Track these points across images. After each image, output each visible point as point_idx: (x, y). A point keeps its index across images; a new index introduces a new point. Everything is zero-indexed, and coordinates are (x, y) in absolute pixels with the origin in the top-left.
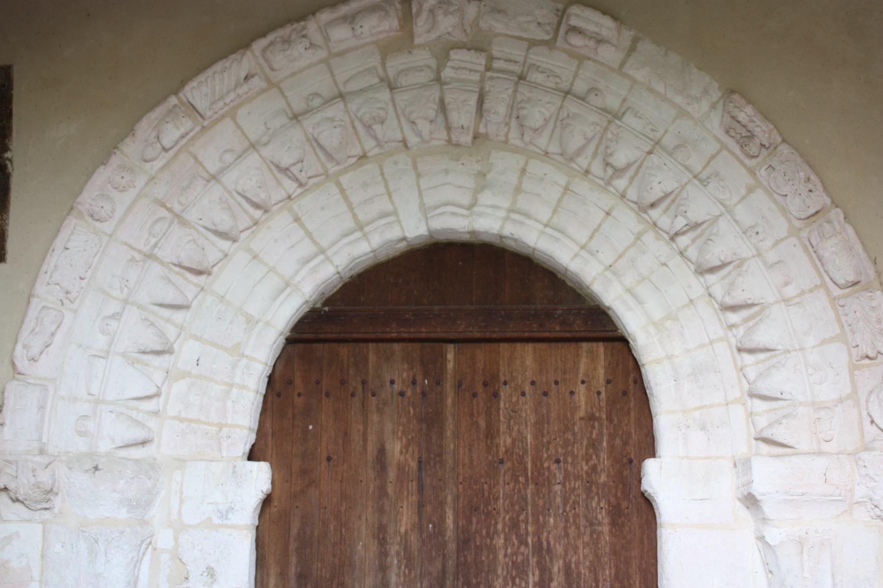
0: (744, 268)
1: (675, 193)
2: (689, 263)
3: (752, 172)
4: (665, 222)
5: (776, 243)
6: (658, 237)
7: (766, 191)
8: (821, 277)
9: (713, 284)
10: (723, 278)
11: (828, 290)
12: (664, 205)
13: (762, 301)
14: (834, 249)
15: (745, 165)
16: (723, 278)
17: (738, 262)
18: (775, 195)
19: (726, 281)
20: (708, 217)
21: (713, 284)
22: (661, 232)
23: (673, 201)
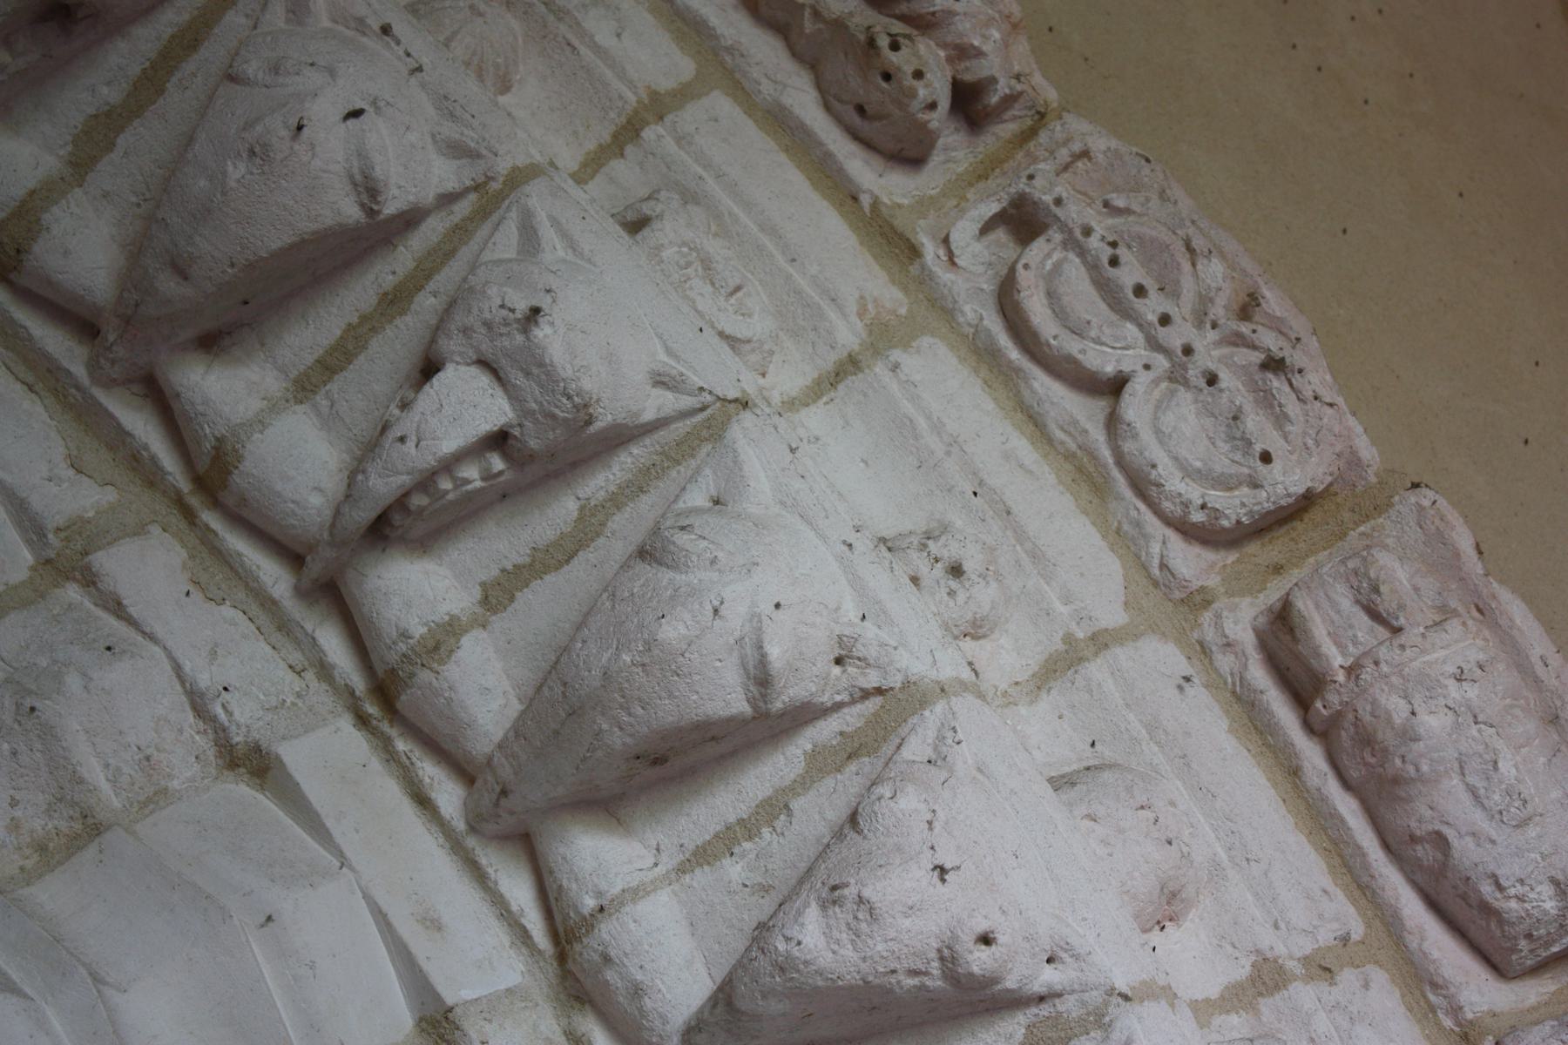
0: (916, 748)
1: (432, 230)
2: (430, 771)
3: (892, 242)
4: (300, 462)
5: (1062, 663)
6: (217, 574)
7: (983, 354)
8: (1363, 889)
9: (636, 893)
10: (703, 856)
11: (1418, 981)
12: (310, 334)
13: (1049, 977)
14: (1472, 692)
15: (846, 196)
16: (703, 856)
17: (851, 718)
18: (1043, 385)
19: (734, 870)
20: (657, 403)
21: (636, 893)
22: (237, 543)
23: (395, 301)
